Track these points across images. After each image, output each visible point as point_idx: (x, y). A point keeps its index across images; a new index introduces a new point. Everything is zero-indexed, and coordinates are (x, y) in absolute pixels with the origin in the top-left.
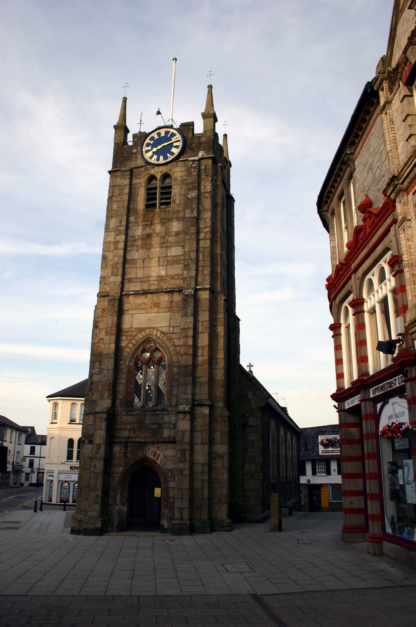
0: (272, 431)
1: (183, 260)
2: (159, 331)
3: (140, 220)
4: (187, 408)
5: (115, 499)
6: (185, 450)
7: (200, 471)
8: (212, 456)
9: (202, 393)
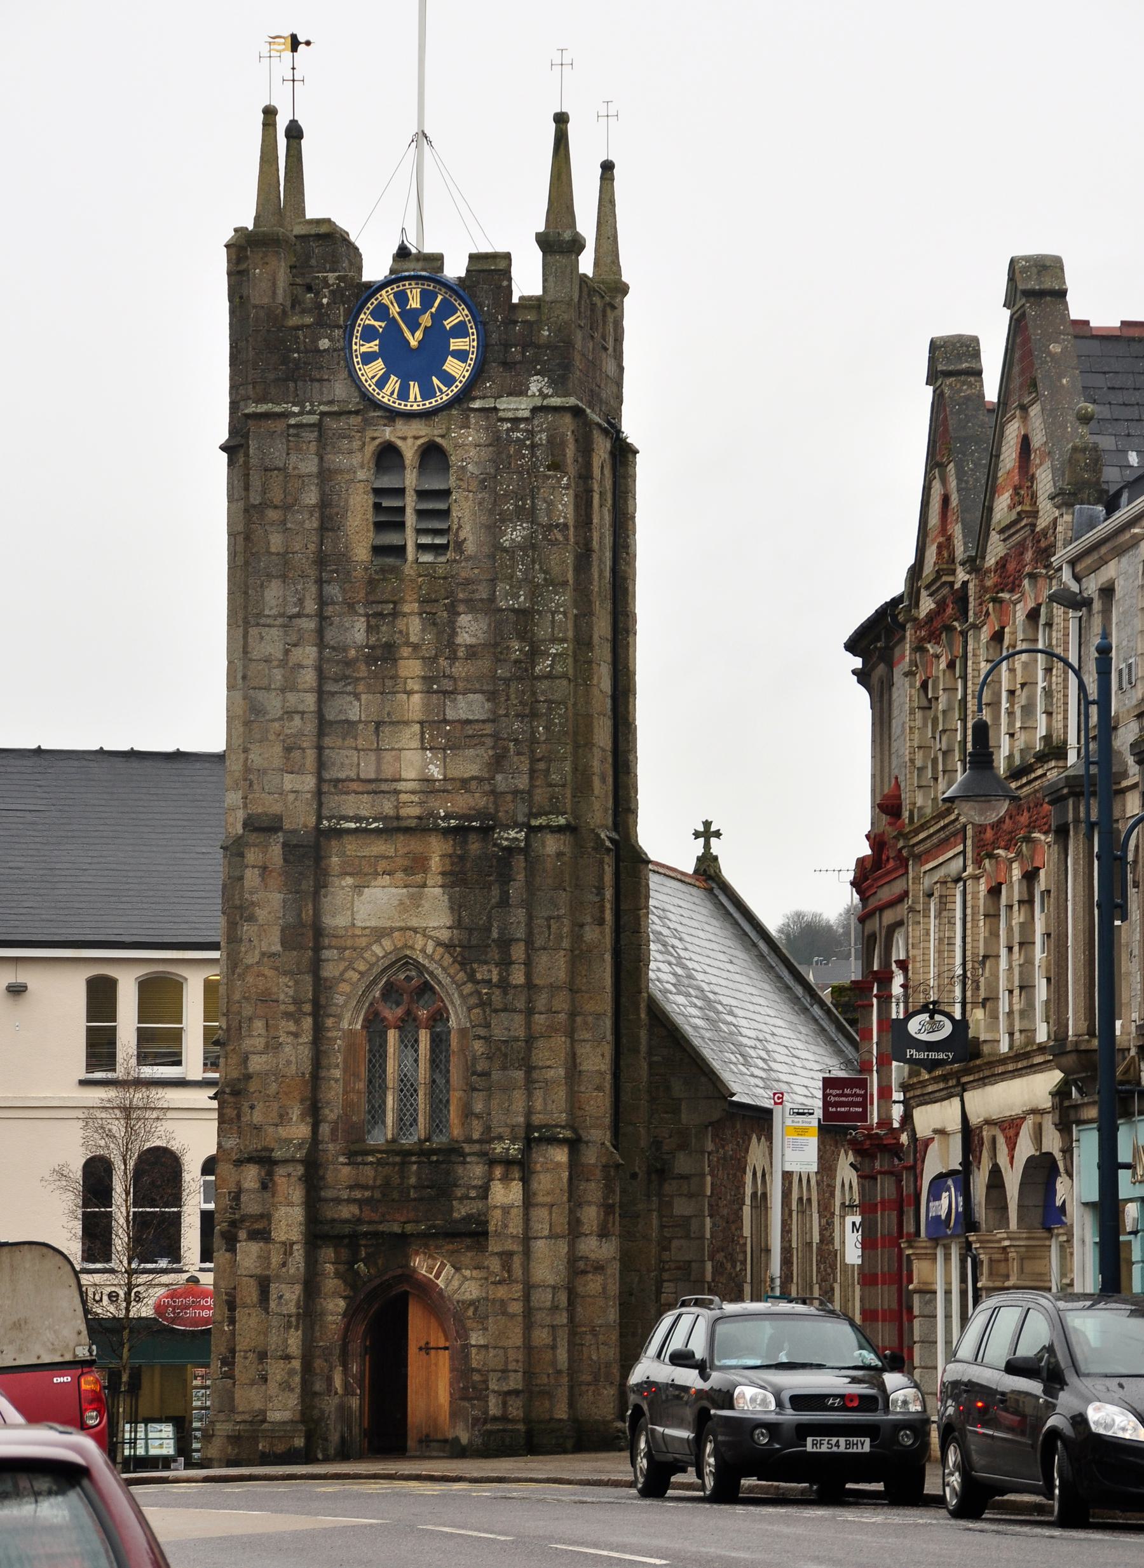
0: (755, 1174)
1: (491, 735)
2: (431, 937)
4: (514, 1149)
5: (329, 1380)
6: (510, 1254)
7: (548, 1304)
8: (576, 1267)
9: (549, 1108)
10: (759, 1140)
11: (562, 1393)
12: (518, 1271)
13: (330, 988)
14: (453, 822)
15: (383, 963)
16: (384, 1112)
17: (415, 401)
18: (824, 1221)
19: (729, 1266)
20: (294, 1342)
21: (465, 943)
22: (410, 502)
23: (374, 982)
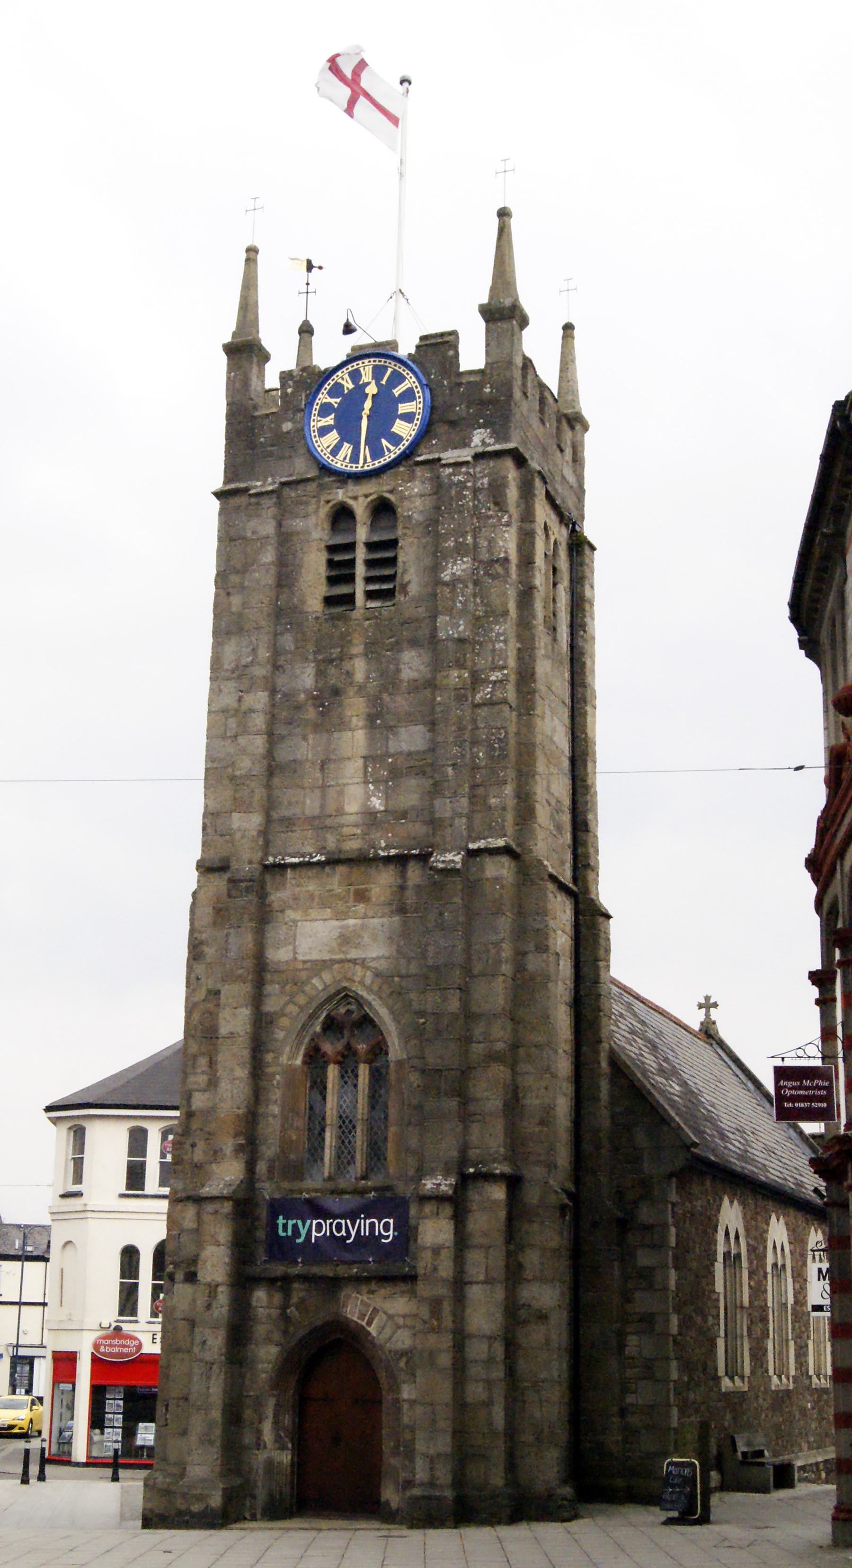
2: (368, 968)
3: (311, 648)
10: (731, 1202)
11: (498, 1454)
12: (448, 1321)
13: (271, 1022)
14: (393, 852)
15: (323, 996)
16: (323, 1148)
17: (367, 463)
18: (797, 1286)
19: (699, 1319)
20: (216, 1390)
21: (404, 972)
22: (361, 554)
23: (312, 1017)
